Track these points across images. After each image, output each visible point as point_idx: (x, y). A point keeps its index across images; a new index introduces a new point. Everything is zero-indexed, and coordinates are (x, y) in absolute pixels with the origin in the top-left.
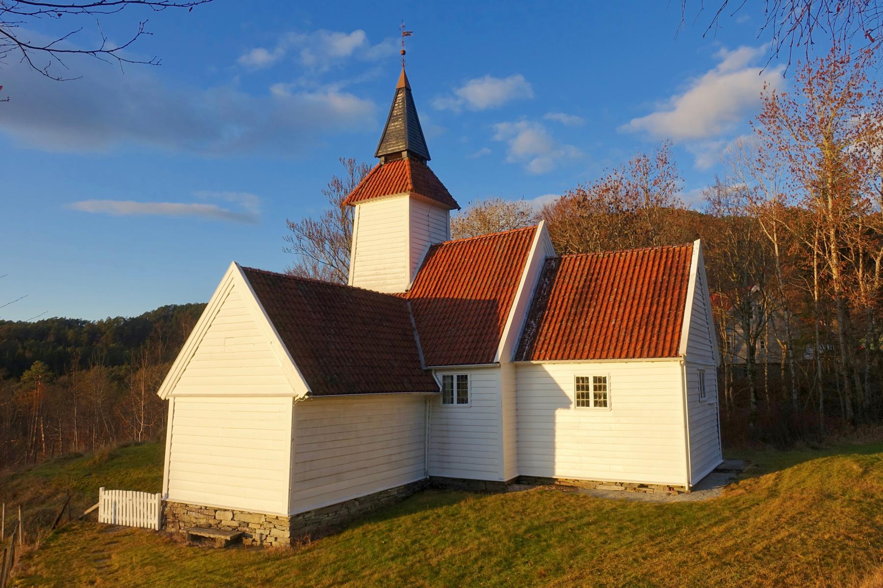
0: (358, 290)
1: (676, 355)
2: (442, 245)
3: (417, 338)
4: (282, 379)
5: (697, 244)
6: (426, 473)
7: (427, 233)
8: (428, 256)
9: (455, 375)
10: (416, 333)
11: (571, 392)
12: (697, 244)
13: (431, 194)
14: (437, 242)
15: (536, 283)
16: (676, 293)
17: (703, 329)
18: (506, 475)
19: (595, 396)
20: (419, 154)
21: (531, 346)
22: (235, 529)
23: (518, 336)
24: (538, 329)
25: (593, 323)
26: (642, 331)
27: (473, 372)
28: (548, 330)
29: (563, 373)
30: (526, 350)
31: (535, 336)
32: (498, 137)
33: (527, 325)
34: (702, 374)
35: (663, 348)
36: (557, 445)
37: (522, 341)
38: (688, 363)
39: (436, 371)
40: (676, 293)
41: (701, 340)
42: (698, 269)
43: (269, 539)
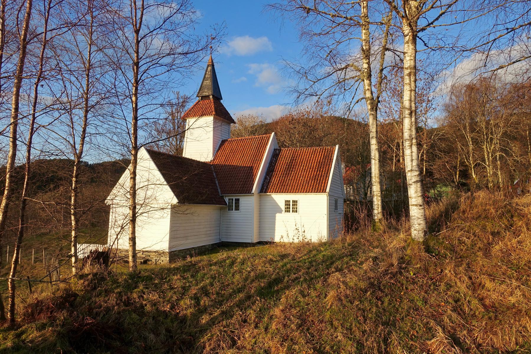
0: (186, 158)
1: (325, 192)
2: (227, 140)
3: (217, 182)
4: (167, 196)
5: (337, 147)
6: (220, 240)
7: (220, 134)
8: (220, 145)
9: (234, 198)
10: (216, 180)
11: (283, 206)
12: (337, 147)
13: (222, 116)
14: (225, 139)
15: (270, 160)
16: (327, 167)
17: (338, 182)
18: (255, 241)
19: (293, 208)
20: (217, 97)
21: (267, 187)
22: (143, 258)
23: (262, 183)
24: (270, 180)
25: (293, 178)
26: (313, 182)
27: (242, 197)
28: (275, 180)
29: (280, 199)
30: (264, 189)
31: (269, 183)
32: (251, 72)
33: (266, 178)
34: (336, 202)
35: (319, 189)
36: (276, 228)
37: (263, 185)
38: (330, 195)
39: (226, 196)
40: (327, 167)
41: (337, 187)
42: (337, 156)
43: (159, 261)
